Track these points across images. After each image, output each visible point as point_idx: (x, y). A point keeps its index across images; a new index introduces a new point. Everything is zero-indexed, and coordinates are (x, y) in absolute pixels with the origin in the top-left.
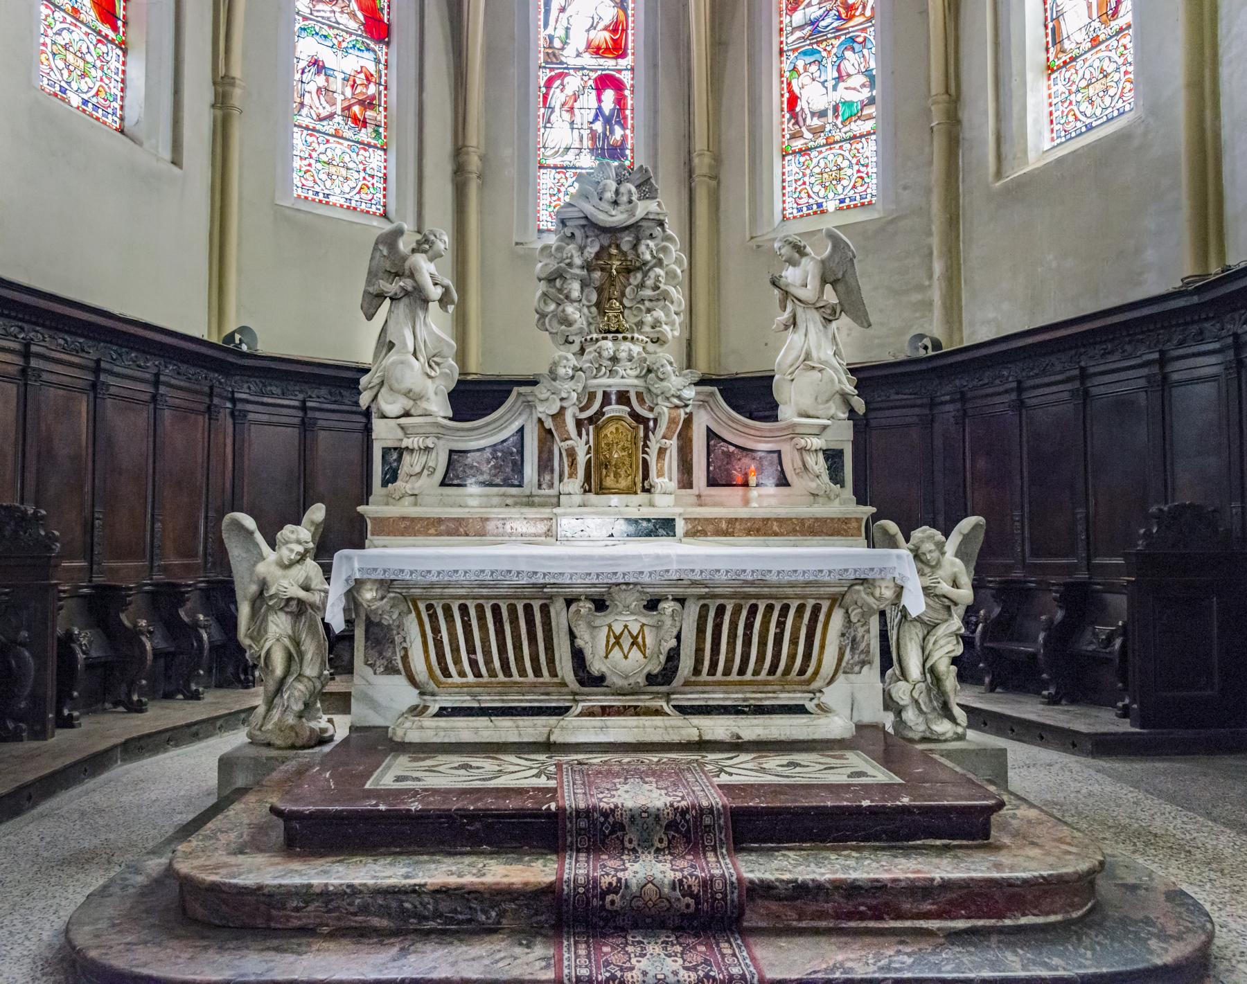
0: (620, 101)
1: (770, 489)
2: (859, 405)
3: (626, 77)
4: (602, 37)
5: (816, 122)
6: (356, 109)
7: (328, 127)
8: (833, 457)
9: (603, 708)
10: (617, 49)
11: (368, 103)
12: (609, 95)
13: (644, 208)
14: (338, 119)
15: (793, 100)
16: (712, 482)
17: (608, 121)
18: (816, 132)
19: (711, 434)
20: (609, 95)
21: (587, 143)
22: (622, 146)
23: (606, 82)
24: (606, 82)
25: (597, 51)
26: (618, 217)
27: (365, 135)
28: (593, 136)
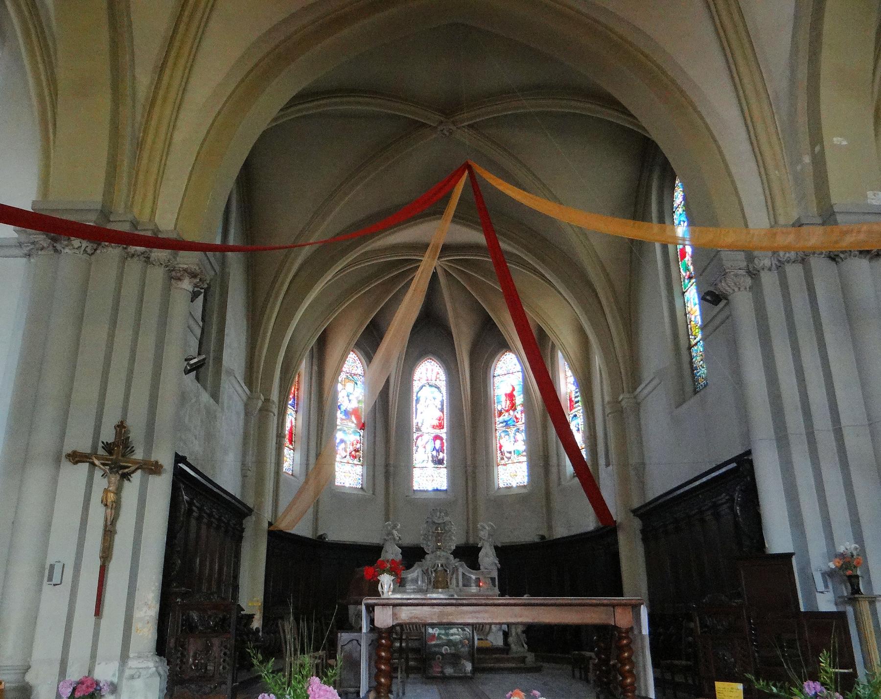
0: (442, 444)
1: (795, 215)
2: (499, 566)
3: (444, 436)
4: (436, 423)
5: (508, 455)
6: (353, 453)
7: (345, 460)
8: (493, 579)
9: (277, 436)
10: (440, 426)
11: (357, 451)
12: (438, 442)
13: (447, 519)
14: (348, 457)
15: (501, 447)
16: (464, 586)
17: (437, 451)
18: (509, 458)
19: (463, 574)
20: (438, 442)
21: (431, 459)
22: (443, 460)
23: (437, 437)
24: (437, 437)
25: (434, 427)
26: (440, 521)
27: (356, 461)
28: (433, 456)
